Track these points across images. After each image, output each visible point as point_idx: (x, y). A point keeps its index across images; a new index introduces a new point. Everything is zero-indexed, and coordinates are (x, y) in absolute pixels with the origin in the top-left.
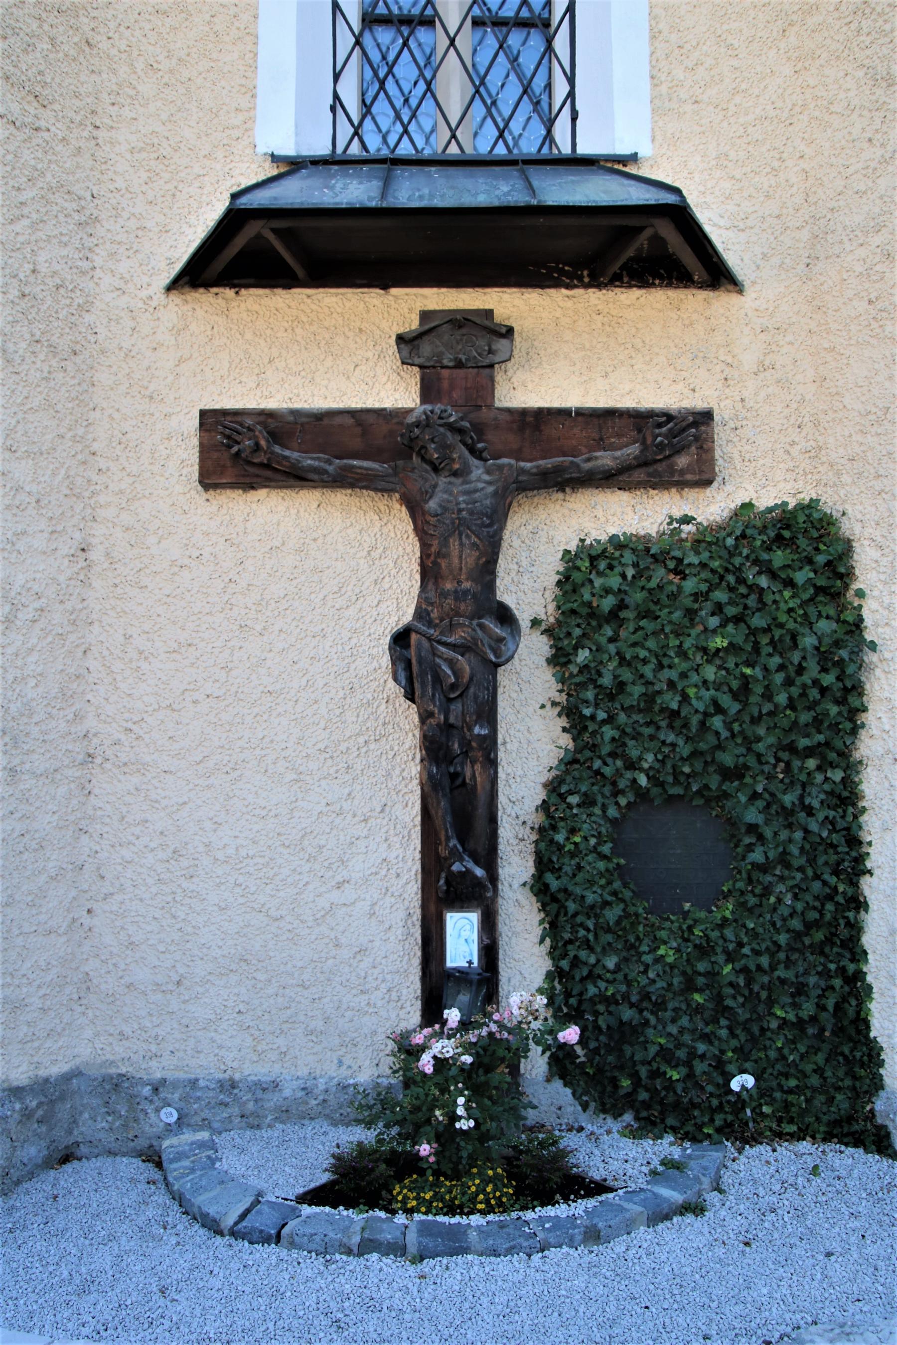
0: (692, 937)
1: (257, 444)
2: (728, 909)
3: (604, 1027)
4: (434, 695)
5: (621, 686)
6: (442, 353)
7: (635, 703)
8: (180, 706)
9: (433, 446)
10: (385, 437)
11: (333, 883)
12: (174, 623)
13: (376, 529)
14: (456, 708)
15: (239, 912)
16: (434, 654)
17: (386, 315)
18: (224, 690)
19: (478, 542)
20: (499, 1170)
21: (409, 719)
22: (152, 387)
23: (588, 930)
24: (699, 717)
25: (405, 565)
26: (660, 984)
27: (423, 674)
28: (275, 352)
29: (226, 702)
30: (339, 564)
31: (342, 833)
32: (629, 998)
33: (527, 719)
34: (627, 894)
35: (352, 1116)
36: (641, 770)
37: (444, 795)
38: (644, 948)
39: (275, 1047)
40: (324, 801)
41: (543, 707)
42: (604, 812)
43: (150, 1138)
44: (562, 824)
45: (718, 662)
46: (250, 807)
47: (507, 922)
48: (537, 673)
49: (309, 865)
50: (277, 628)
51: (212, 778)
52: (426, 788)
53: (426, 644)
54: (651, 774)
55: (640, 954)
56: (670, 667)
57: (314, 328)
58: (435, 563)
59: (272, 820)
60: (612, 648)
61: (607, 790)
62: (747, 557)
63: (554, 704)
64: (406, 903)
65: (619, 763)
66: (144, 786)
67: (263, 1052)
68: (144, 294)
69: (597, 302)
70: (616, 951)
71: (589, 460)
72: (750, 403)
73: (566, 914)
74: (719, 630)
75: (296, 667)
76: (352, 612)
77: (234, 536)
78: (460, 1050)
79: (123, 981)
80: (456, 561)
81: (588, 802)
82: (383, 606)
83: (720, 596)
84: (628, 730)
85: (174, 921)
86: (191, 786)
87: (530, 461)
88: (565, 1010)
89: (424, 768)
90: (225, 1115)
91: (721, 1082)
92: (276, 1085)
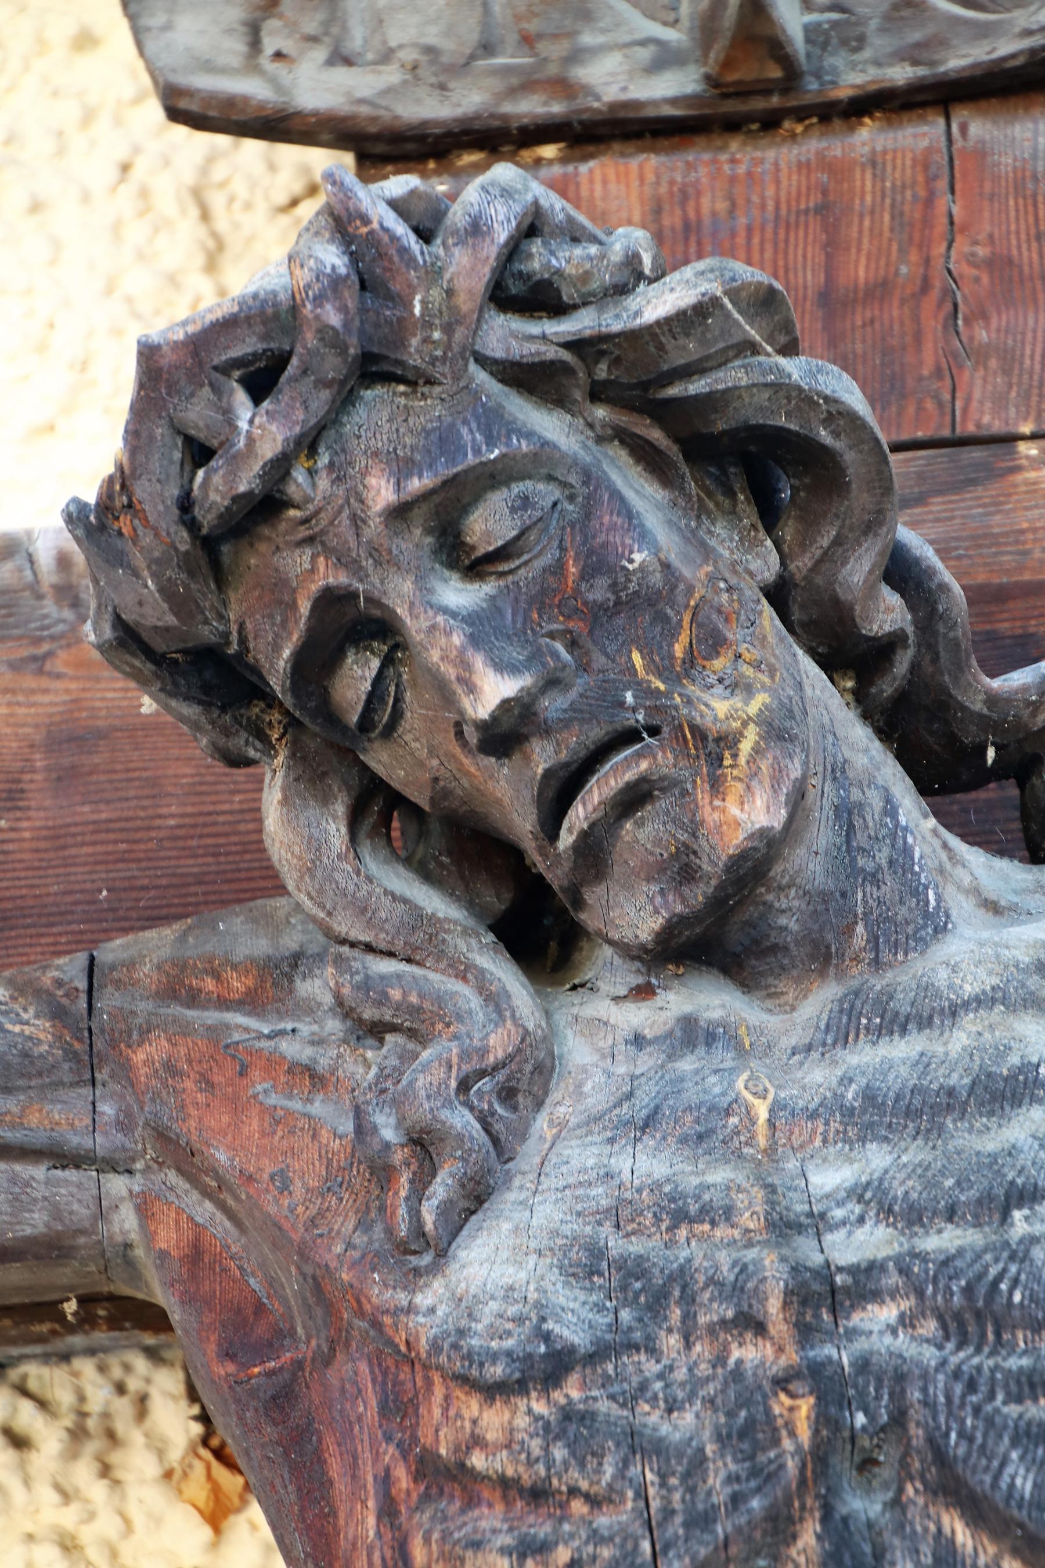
9: (458, 594)
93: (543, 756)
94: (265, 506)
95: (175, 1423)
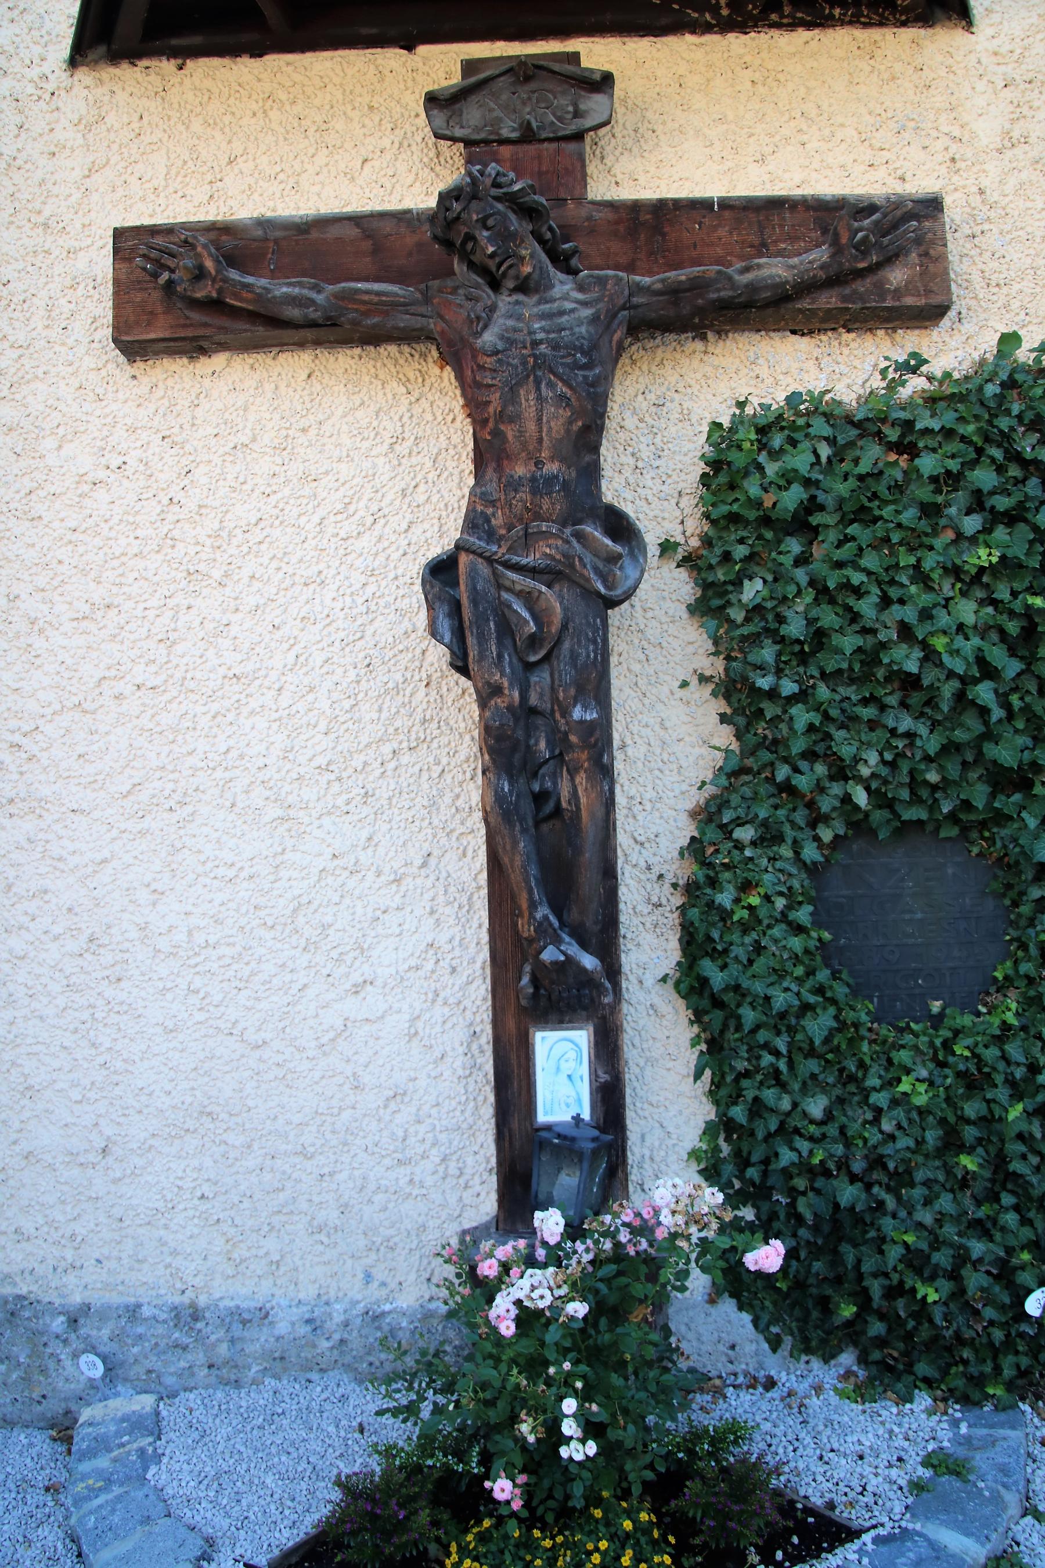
0: (951, 1059)
1: (201, 268)
2: (1011, 1009)
3: (809, 1216)
4: (500, 656)
5: (819, 637)
6: (499, 120)
7: (845, 666)
8: (96, 705)
9: (486, 234)
10: (410, 254)
11: (348, 986)
12: (85, 573)
13: (403, 409)
14: (541, 679)
15: (197, 1035)
16: (500, 587)
17: (410, 84)
18: (164, 677)
19: (569, 393)
20: (644, 1516)
21: (465, 712)
22: (47, 213)
23: (777, 1054)
24: (955, 684)
25: (451, 464)
26: (904, 1142)
27: (480, 619)
28: (238, 147)
29: (167, 696)
30: (343, 466)
31: (359, 904)
32: (848, 1167)
33: (660, 706)
34: (840, 991)
35: (388, 1367)
36: (859, 779)
37: (524, 831)
38: (873, 1081)
39: (261, 1252)
40: (328, 852)
41: (684, 684)
42: (797, 853)
43: (66, 1399)
44: (727, 875)
45: (980, 594)
46: (210, 865)
47: (637, 1041)
48: (672, 629)
49: (307, 956)
50: (246, 573)
51: (148, 818)
52: (491, 820)
53: (484, 569)
54: (874, 785)
55: (866, 1093)
56: (902, 602)
57: (298, 109)
58: (497, 433)
59: (245, 884)
60: (801, 575)
61: (800, 817)
62: (1020, 417)
63: (703, 679)
64: (468, 1014)
65: (821, 769)
66: (41, 835)
67: (242, 1261)
68: (34, 73)
69: (742, 51)
70: (825, 1088)
71: (747, 269)
72: (993, 196)
73: (739, 1028)
74: (981, 537)
75: (278, 634)
76: (366, 542)
77: (176, 430)
78: (564, 1291)
79: (17, 1148)
80: (531, 426)
81: (769, 836)
82: (417, 530)
83: (984, 477)
84: (834, 713)
85: (93, 1052)
86: (115, 833)
87: (650, 273)
88: (737, 1185)
89: (487, 783)
90: (183, 1364)
91: (1007, 1300)
92: (264, 1314)
93: (497, 260)
94: (458, 218)
95: (435, 354)
